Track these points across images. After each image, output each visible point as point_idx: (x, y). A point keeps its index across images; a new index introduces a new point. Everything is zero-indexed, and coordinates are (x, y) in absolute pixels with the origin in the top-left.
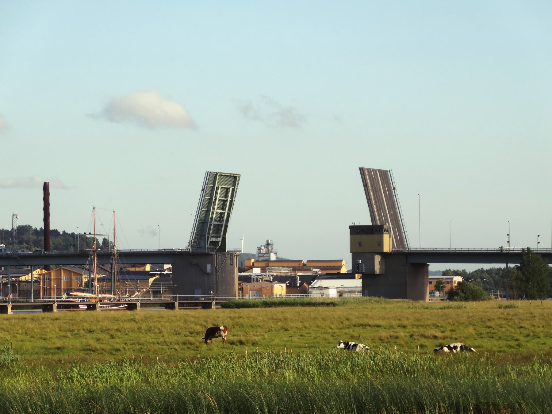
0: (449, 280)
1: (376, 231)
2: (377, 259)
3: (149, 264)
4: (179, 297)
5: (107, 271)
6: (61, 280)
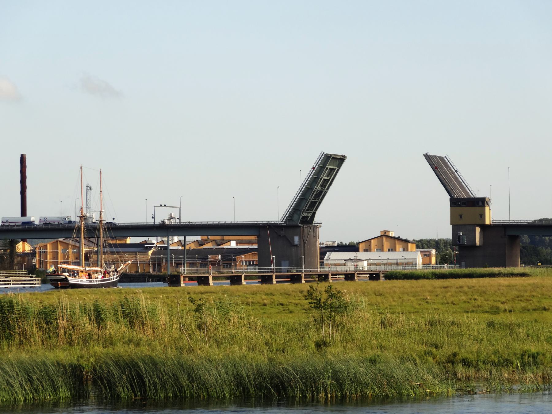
0: (428, 253)
1: (478, 203)
2: (478, 230)
3: (129, 237)
4: (276, 269)
5: (93, 242)
6: (57, 252)
